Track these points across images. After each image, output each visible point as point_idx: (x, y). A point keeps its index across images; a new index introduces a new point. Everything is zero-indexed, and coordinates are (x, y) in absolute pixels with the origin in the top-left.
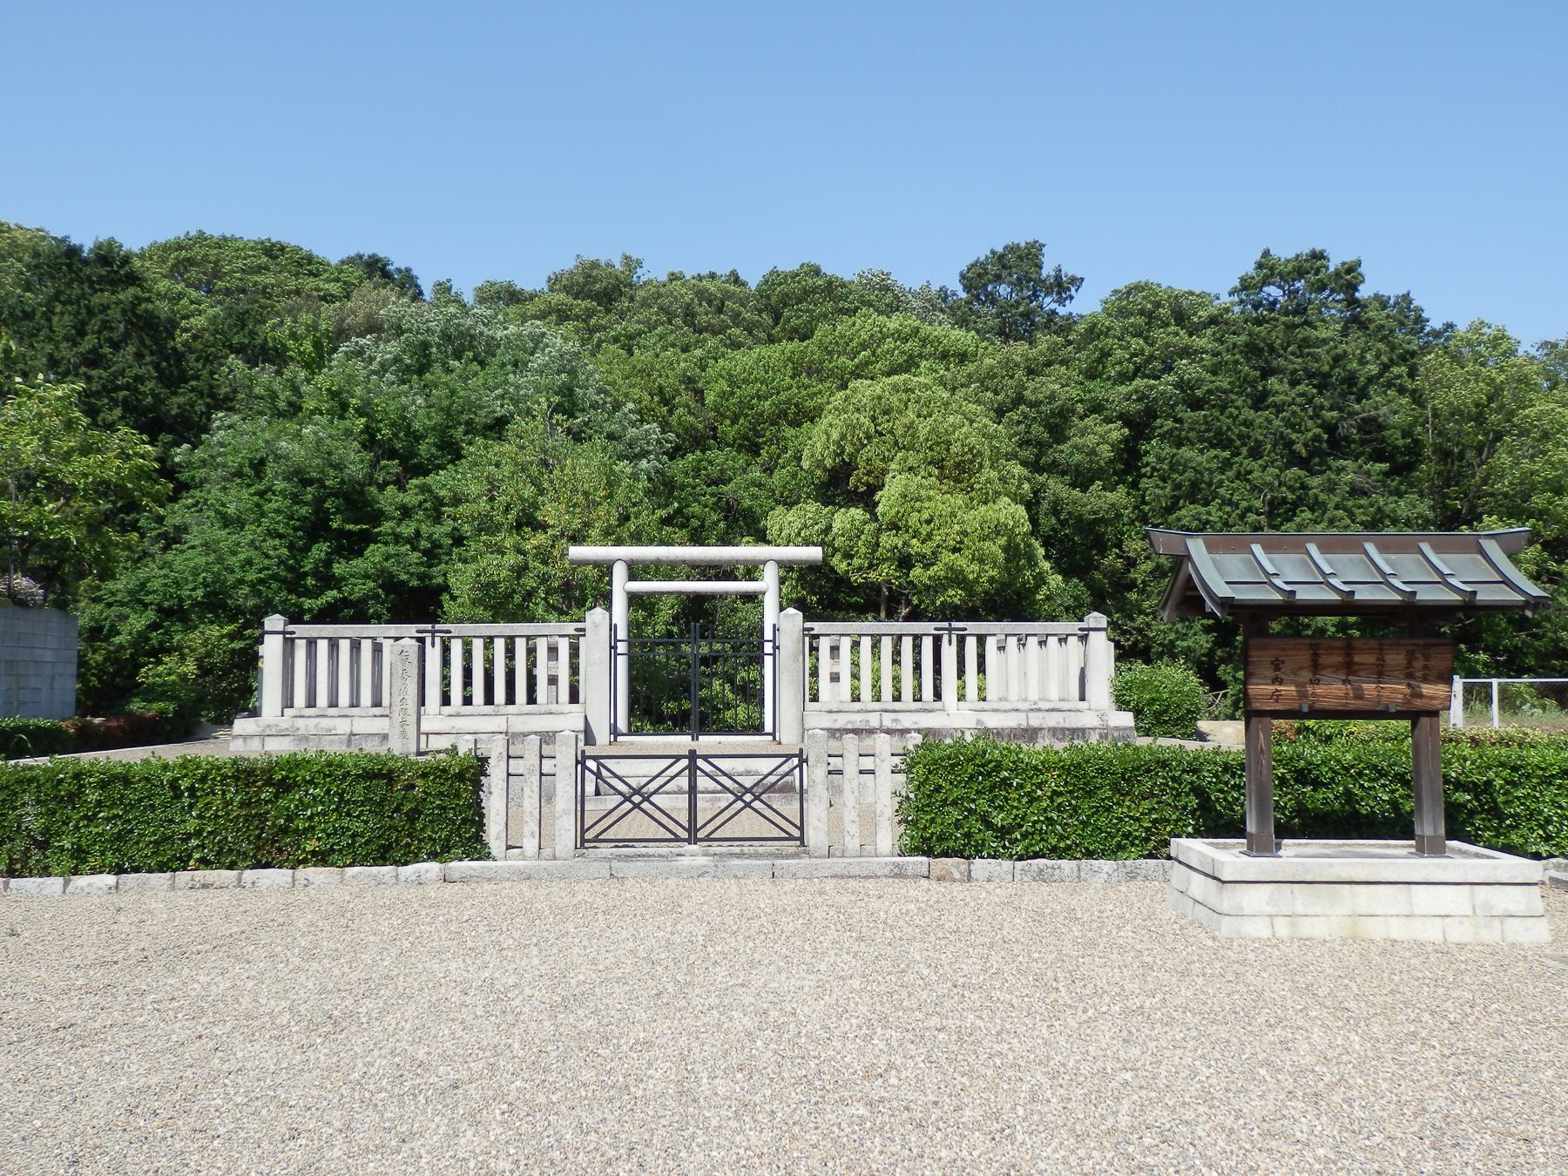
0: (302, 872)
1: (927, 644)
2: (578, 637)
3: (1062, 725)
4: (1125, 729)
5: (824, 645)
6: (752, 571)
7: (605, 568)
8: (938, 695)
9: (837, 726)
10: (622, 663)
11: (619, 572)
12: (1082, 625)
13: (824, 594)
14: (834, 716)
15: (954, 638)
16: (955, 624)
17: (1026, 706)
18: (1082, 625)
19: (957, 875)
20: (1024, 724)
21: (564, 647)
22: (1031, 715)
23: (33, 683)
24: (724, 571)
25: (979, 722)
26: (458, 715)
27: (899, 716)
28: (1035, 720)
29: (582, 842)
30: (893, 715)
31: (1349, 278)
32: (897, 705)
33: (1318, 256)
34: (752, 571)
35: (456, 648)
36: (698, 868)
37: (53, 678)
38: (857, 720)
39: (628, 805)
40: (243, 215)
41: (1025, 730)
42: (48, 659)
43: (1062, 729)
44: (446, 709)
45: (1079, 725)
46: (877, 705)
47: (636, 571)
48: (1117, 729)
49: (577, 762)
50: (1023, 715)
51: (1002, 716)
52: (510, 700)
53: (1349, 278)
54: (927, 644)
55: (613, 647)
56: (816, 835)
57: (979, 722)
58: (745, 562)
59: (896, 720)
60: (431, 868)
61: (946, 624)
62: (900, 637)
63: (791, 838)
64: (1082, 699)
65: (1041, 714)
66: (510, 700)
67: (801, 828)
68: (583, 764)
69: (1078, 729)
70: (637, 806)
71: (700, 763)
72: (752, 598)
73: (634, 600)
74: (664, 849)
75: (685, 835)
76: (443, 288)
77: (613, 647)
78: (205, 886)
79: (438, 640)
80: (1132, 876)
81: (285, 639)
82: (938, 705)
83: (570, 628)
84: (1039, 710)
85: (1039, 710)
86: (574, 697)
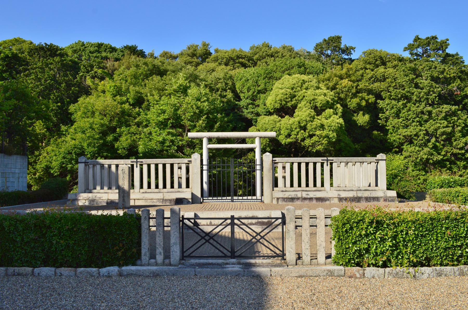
0: (59, 270)
1: (318, 166)
2: (188, 164)
3: (370, 196)
4: (393, 197)
5: (280, 166)
6: (252, 140)
7: (201, 140)
8: (322, 185)
9: (285, 197)
10: (205, 173)
11: (205, 141)
12: (376, 158)
13: (275, 148)
14: (284, 193)
15: (329, 163)
16: (329, 158)
17: (356, 189)
18: (376, 158)
19: (358, 275)
20: (356, 196)
21: (184, 167)
22: (358, 192)
23: (11, 180)
24: (243, 141)
25: (339, 195)
26: (146, 193)
27: (309, 193)
28: (360, 194)
29: (183, 257)
30: (306, 193)
31: (444, 45)
32: (307, 189)
33: (435, 38)
34: (252, 140)
35: (145, 168)
36: (236, 272)
37: (19, 178)
38: (292, 195)
39: (203, 241)
40: (92, 38)
41: (356, 198)
42: (17, 172)
43: (370, 197)
44: (142, 190)
45: (376, 196)
46: (300, 189)
47: (210, 140)
48: (390, 197)
49: (180, 221)
50: (355, 192)
51: (347, 192)
52: (165, 187)
53: (444, 45)
54: (318, 166)
55: (202, 168)
56: (290, 256)
57: (339, 195)
58: (250, 138)
59: (308, 194)
60: (114, 269)
61: (326, 158)
62: (293, 163)
63: (278, 256)
64: (377, 185)
65: (362, 192)
66: (165, 187)
67: (283, 251)
68: (183, 221)
69: (376, 197)
70: (207, 241)
71: (236, 221)
72: (252, 150)
73: (210, 150)
74: (220, 261)
75: (229, 254)
76: (152, 55)
77: (202, 168)
78: (19, 274)
79: (138, 165)
80: (440, 274)
81: (86, 165)
82: (323, 188)
83: (186, 160)
84: (361, 190)
85: (361, 190)
86: (188, 186)
